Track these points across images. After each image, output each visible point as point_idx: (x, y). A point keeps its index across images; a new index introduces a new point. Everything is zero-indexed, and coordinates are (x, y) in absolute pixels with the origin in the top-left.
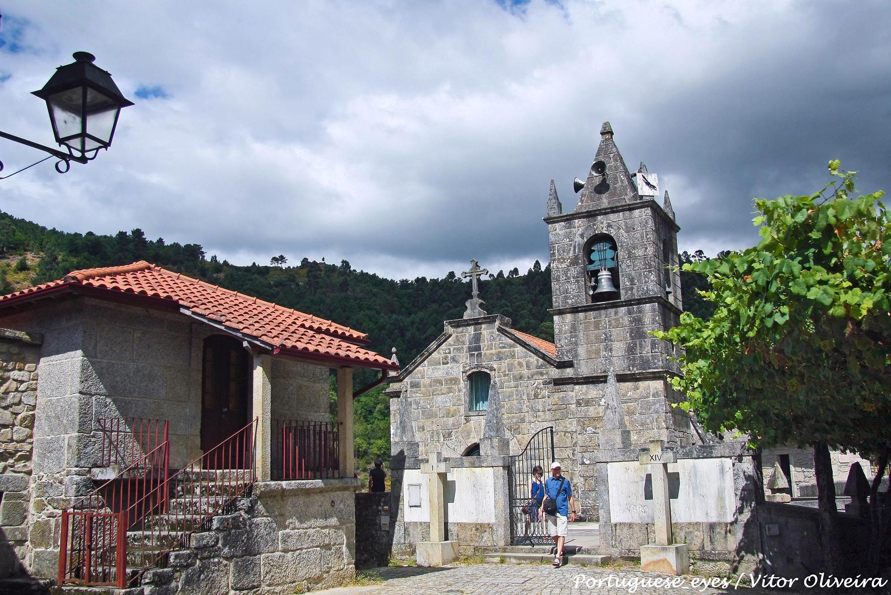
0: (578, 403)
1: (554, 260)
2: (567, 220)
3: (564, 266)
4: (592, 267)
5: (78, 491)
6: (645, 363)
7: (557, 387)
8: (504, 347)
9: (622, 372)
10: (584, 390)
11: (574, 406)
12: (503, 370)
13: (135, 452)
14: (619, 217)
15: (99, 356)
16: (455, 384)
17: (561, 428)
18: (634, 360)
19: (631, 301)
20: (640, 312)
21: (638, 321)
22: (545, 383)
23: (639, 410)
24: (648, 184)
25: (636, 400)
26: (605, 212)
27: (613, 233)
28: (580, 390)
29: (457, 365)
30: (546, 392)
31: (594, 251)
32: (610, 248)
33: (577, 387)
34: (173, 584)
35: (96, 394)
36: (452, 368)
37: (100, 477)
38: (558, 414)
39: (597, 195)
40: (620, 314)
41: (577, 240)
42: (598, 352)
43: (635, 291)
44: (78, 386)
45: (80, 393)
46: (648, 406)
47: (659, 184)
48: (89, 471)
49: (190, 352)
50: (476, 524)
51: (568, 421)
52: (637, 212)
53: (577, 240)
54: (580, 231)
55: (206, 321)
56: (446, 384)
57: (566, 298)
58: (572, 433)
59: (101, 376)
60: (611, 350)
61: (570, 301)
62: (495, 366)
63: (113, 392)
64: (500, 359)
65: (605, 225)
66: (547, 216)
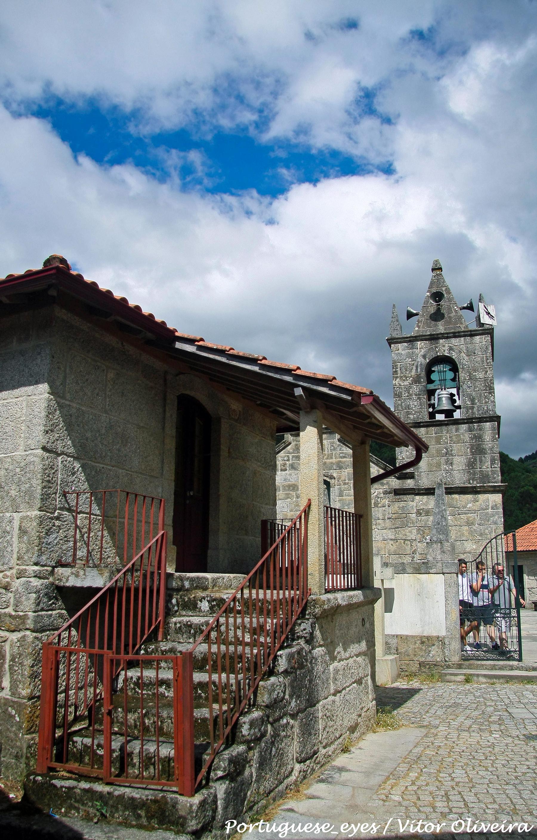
0: (419, 513)
1: (397, 378)
2: (410, 341)
3: (406, 383)
4: (431, 387)
5: (38, 604)
6: (485, 477)
7: (398, 497)
8: (344, 457)
9: (462, 485)
10: (424, 501)
11: (414, 515)
12: (343, 478)
13: (105, 546)
14: (460, 342)
15: (68, 396)
16: (293, 490)
17: (401, 536)
18: (474, 474)
19: (472, 419)
20: (480, 430)
21: (479, 438)
22: (385, 493)
23: (478, 521)
24: (488, 313)
25: (475, 512)
26: (446, 336)
27: (454, 355)
28: (419, 501)
29: (296, 472)
30: (386, 502)
31: (434, 371)
32: (450, 370)
33: (417, 497)
34: (247, 773)
35: (63, 453)
36: (290, 475)
37: (72, 582)
38: (398, 523)
39: (433, 322)
40: (461, 431)
41: (419, 360)
42: (439, 465)
43: (475, 410)
44: (39, 437)
45: (44, 448)
46: (486, 518)
47: (496, 315)
48: (52, 573)
49: (164, 411)
50: (421, 637)
51: (408, 530)
52: (477, 338)
53: (419, 360)
54: (423, 352)
55: (224, 360)
56: (284, 489)
57: (408, 413)
58: (411, 541)
59: (70, 427)
60: (452, 464)
61: (412, 417)
62: (335, 475)
63: (83, 453)
64: (341, 468)
65: (446, 348)
66: (389, 337)
